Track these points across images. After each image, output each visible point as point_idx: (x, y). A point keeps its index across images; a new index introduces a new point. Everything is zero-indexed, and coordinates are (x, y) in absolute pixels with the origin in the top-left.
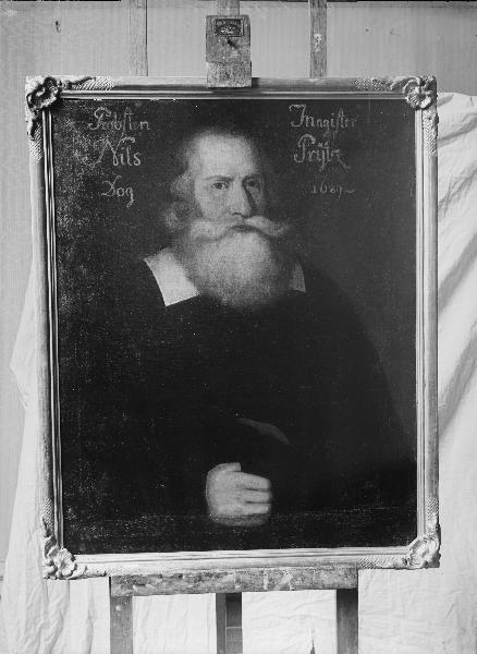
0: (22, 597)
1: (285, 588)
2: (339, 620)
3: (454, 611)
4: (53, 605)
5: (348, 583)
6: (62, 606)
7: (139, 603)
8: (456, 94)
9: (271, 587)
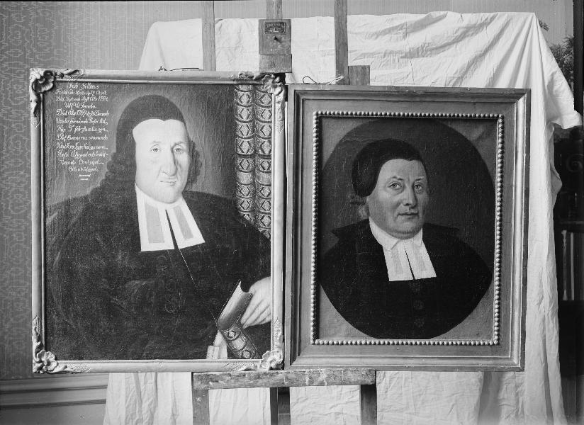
0: (123, 398)
1: (322, 384)
2: (362, 409)
3: (454, 411)
4: (145, 405)
5: (369, 381)
6: (152, 405)
7: (213, 394)
8: (450, 13)
9: (311, 383)
